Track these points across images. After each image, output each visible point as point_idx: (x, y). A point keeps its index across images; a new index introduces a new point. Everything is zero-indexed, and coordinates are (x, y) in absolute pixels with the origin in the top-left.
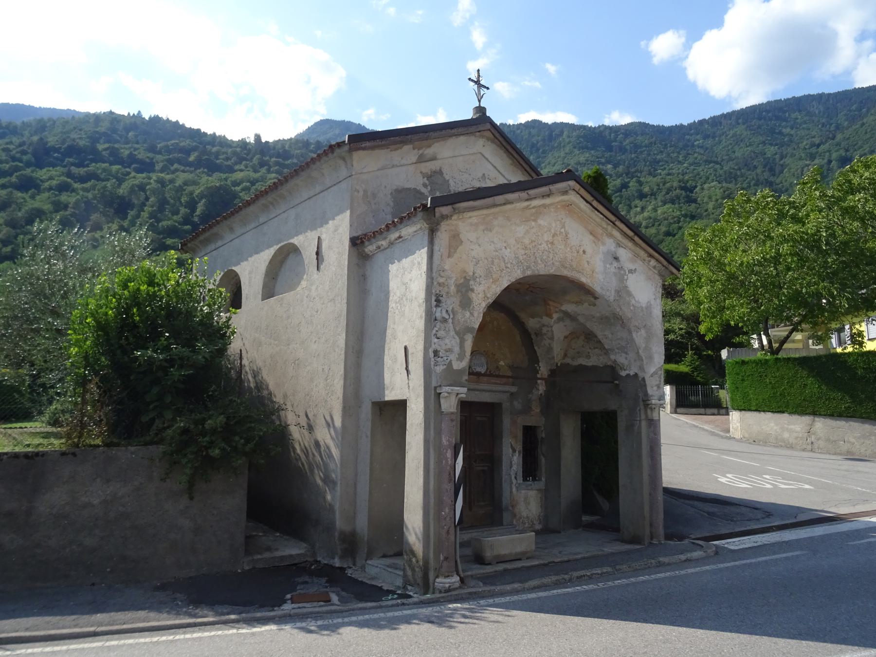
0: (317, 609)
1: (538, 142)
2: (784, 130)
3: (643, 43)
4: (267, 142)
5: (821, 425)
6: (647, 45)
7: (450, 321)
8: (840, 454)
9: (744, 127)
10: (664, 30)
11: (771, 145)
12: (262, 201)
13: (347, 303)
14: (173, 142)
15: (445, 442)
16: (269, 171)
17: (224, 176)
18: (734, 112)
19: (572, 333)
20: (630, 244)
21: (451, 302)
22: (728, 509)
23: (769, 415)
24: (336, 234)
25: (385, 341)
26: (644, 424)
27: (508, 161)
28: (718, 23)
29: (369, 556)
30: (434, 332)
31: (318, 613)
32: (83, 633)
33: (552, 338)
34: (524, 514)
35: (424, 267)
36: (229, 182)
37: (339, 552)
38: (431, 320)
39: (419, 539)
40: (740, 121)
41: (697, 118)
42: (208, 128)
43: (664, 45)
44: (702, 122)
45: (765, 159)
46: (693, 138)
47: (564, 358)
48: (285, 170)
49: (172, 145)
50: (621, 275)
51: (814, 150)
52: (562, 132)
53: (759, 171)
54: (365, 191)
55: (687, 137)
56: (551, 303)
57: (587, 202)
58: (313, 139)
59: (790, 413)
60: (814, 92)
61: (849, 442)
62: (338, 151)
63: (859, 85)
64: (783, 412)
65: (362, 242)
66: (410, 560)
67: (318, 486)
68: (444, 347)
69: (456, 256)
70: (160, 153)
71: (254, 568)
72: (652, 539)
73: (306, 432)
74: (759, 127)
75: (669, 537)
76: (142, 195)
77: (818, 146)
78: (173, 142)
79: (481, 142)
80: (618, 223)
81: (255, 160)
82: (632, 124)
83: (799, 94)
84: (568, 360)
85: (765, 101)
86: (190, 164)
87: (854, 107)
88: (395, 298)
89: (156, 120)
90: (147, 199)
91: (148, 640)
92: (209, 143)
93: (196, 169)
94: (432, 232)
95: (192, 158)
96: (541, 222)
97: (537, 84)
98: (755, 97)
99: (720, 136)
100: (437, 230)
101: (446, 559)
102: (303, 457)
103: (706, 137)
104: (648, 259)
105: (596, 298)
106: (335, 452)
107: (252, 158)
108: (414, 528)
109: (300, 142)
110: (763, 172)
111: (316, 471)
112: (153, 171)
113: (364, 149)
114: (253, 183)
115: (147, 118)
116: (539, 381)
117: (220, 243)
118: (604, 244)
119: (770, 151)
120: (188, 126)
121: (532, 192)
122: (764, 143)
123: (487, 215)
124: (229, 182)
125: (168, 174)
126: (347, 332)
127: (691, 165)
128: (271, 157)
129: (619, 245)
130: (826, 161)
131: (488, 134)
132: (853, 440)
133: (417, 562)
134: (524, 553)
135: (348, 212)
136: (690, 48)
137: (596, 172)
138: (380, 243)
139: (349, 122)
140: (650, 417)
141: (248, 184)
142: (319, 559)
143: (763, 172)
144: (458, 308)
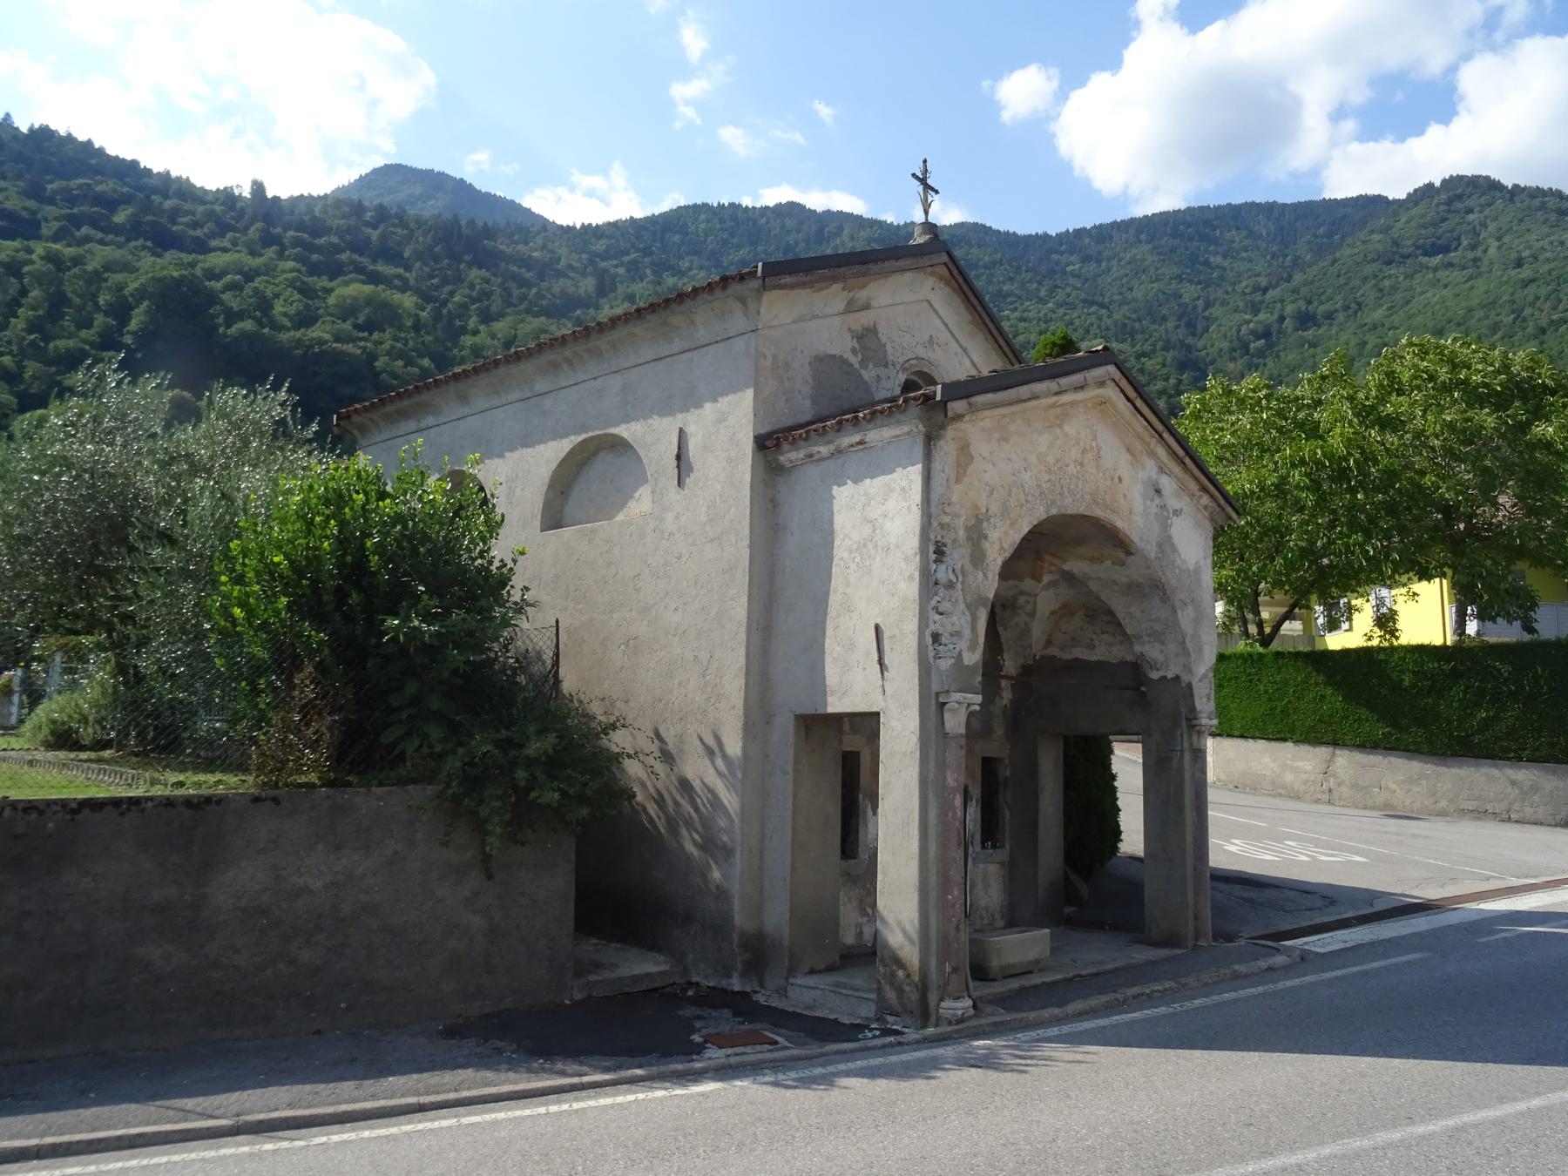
0: (760, 1056)
1: (797, 242)
2: (1212, 259)
3: (985, 84)
4: (276, 199)
5: (1346, 761)
6: (993, 89)
7: (959, 586)
8: (1373, 808)
9: (1147, 247)
10: (1023, 65)
11: (1191, 282)
12: (549, 356)
13: (751, 547)
14: (81, 181)
15: (951, 781)
16: (281, 255)
17: (187, 258)
18: (1132, 220)
19: (1064, 606)
20: (1177, 470)
21: (958, 556)
22: (1269, 894)
23: (1262, 744)
24: (724, 427)
25: (825, 614)
26: (1187, 756)
27: (966, 316)
28: (1113, 63)
29: (792, 971)
30: (933, 603)
31: (775, 1060)
32: (393, 1108)
33: (1032, 614)
34: (983, 903)
35: (916, 495)
36: (198, 271)
37: (739, 965)
38: (929, 585)
39: (911, 941)
40: (1143, 237)
41: (1072, 225)
42: (155, 160)
43: (1022, 90)
44: (1080, 233)
45: (1180, 305)
46: (1064, 259)
47: (1045, 647)
48: (315, 257)
49: (80, 187)
50: (1164, 517)
51: (1258, 297)
52: (840, 229)
53: (1170, 325)
54: (775, 357)
55: (1055, 257)
56: (1047, 557)
57: (1128, 399)
58: (371, 199)
59: (1296, 742)
60: (1261, 199)
61: (1387, 789)
62: (735, 288)
63: (1328, 195)
64: (1285, 740)
65: (778, 445)
66: (893, 975)
67: (688, 857)
68: (950, 629)
69: (966, 480)
70: (51, 201)
71: (590, 997)
72: (1197, 938)
73: (659, 767)
74: (1173, 250)
75: (1217, 935)
76: (13, 285)
77: (1265, 290)
78: (81, 181)
79: (931, 282)
80: (1166, 435)
81: (254, 233)
82: (963, 224)
83: (1238, 199)
84: (1053, 651)
85: (1183, 207)
86: (117, 230)
87: (1321, 231)
88: (847, 543)
89: (43, 136)
90: (24, 292)
91: (609, 1101)
92: (156, 190)
93: (128, 240)
94: (930, 439)
95: (120, 217)
96: (1068, 429)
97: (798, 137)
98: (1167, 199)
99: (1109, 260)
100: (939, 437)
101: (955, 970)
102: (652, 809)
103: (1086, 259)
104: (1198, 493)
105: (1129, 553)
106: (730, 800)
107: (247, 228)
108: (899, 923)
109: (347, 204)
110: (1177, 327)
111: (684, 832)
112: (39, 237)
113: (782, 287)
114: (249, 276)
115: (24, 130)
116: (1003, 683)
117: (430, 420)
118: (1143, 468)
119: (1189, 292)
120: (111, 151)
121: (1064, 381)
122: (1180, 278)
123: (1004, 416)
124: (198, 271)
125: (69, 245)
126: (750, 596)
127: (1059, 305)
128: (285, 229)
129: (1161, 470)
130: (1276, 316)
131: (943, 270)
132: (1394, 786)
133: (908, 976)
134: (1037, 962)
135: (750, 393)
136: (1066, 98)
137: (1064, 338)
138: (815, 449)
139: (442, 175)
140: (1195, 745)
141: (238, 277)
142: (694, 980)
143: (1177, 327)
144: (969, 567)
